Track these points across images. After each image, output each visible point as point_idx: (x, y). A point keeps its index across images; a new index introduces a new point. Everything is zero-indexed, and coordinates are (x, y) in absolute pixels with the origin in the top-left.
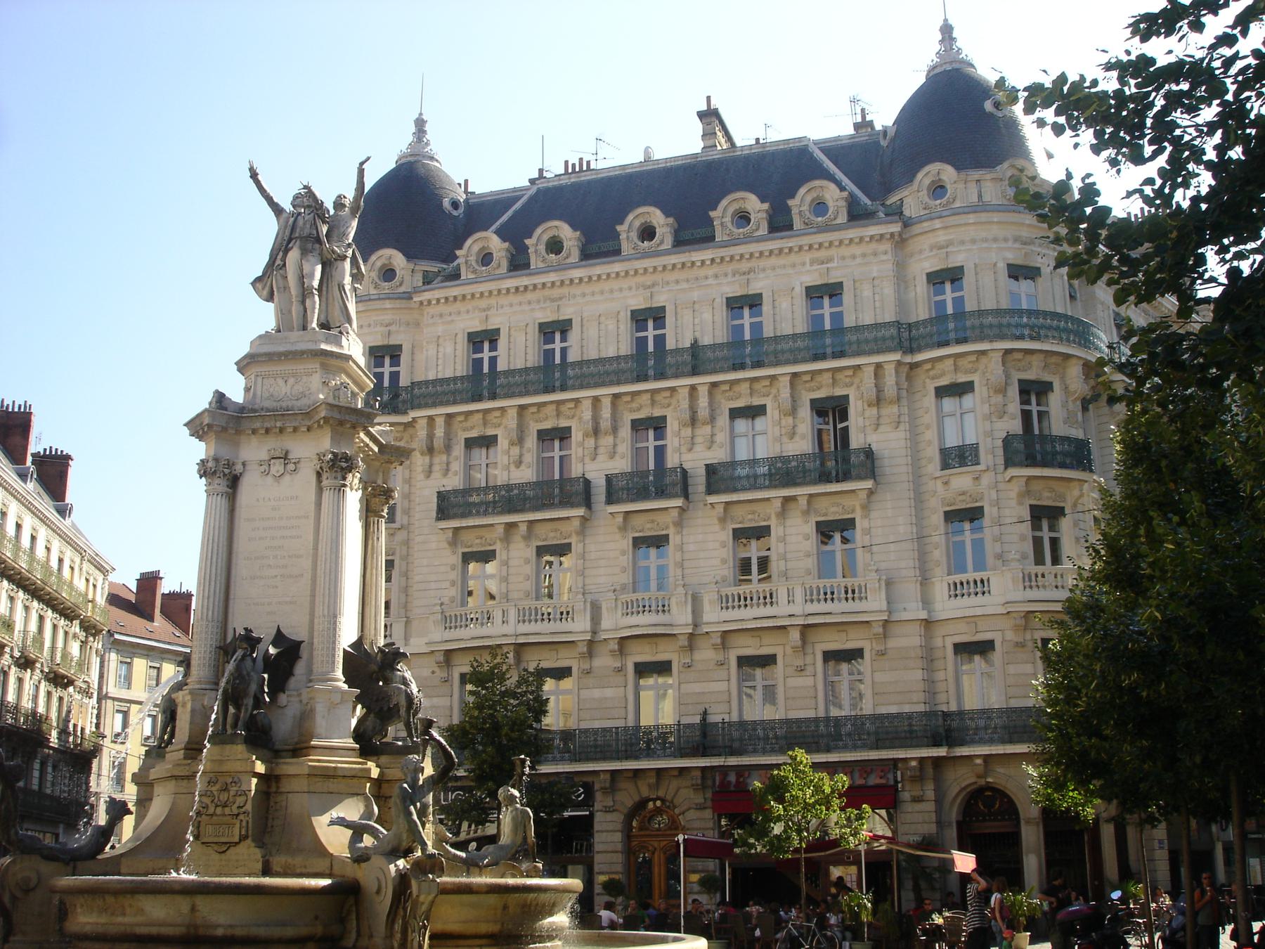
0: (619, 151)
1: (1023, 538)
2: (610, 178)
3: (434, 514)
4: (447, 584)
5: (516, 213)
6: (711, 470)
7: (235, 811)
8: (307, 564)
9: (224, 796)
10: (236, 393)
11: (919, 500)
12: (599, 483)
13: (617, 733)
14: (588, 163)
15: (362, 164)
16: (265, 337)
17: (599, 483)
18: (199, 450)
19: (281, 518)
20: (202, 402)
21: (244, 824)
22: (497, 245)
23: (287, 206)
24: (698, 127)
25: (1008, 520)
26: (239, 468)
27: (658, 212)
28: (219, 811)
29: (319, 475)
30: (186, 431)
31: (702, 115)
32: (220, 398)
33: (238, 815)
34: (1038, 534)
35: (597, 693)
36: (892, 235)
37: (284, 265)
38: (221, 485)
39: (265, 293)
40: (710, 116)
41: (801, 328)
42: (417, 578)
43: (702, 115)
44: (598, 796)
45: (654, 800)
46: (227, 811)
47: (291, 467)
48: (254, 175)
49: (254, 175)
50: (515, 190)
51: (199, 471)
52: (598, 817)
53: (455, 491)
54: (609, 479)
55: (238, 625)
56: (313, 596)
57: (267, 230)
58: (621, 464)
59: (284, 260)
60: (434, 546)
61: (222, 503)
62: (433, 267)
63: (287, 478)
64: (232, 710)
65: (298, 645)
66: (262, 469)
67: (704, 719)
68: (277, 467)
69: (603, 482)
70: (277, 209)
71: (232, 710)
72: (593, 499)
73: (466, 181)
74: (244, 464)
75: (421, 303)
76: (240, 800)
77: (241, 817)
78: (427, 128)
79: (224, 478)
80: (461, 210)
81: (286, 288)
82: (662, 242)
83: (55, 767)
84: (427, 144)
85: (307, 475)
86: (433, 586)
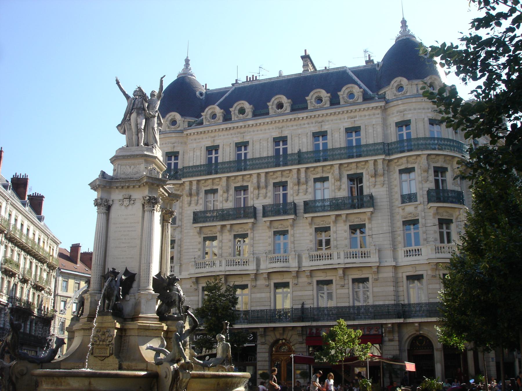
0: (269, 72)
1: (435, 232)
2: (265, 84)
3: (192, 221)
4: (197, 250)
5: (226, 98)
6: (306, 203)
7: (108, 343)
8: (138, 242)
9: (103, 337)
10: (110, 172)
11: (392, 216)
12: (260, 209)
13: (267, 312)
14: (256, 77)
15: (162, 78)
17: (260, 209)
18: (94, 195)
19: (128, 223)
20: (96, 175)
21: (111, 349)
22: (218, 111)
23: (131, 95)
24: (301, 62)
25: (429, 225)
26: (111, 202)
27: (284, 97)
28: (101, 343)
29: (143, 205)
30: (89, 187)
31: (302, 57)
32: (103, 174)
33: (109, 345)
34: (442, 230)
35: (258, 295)
36: (381, 107)
38: (103, 209)
39: (122, 131)
40: (306, 58)
41: (343, 145)
42: (185, 247)
43: (302, 57)
44: (259, 338)
45: (282, 340)
46: (104, 343)
47: (132, 202)
48: (118, 83)
49: (118, 83)
50: (226, 88)
51: (94, 204)
52: (259, 347)
53: (200, 212)
54: (264, 207)
55: (110, 267)
56: (141, 255)
57: (123, 105)
58: (269, 201)
59: (130, 117)
60: (191, 234)
61: (104, 217)
62: (192, 120)
63: (130, 207)
64: (107, 302)
65: (134, 275)
66: (120, 203)
67: (303, 306)
68: (126, 202)
69: (261, 208)
70: (127, 97)
71: (107, 302)
72: (257, 215)
73: (206, 85)
74: (113, 201)
75: (187, 134)
76: (110, 339)
77: (110, 346)
78: (190, 63)
79: (105, 206)
80: (204, 96)
81: (131, 129)
82: (286, 110)
83: (36, 324)
84: (190, 69)
85: (138, 205)
86: (191, 250)
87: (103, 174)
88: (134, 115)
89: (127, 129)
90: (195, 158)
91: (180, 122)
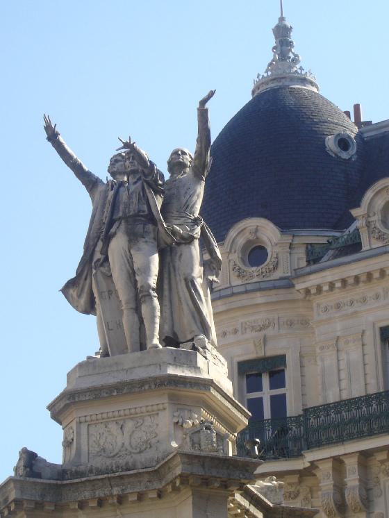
10: (53, 452)
15: (203, 102)
16: (87, 366)
23: (103, 175)
32: (30, 460)
37: (106, 259)
39: (83, 300)
48: (53, 136)
49: (53, 136)
57: (78, 210)
59: (105, 252)
70: (89, 181)
80: (353, 150)
81: (112, 292)
84: (296, 60)
87: (30, 460)
88: (118, 244)
89: (101, 293)
90: (343, 375)
91: (277, 249)
